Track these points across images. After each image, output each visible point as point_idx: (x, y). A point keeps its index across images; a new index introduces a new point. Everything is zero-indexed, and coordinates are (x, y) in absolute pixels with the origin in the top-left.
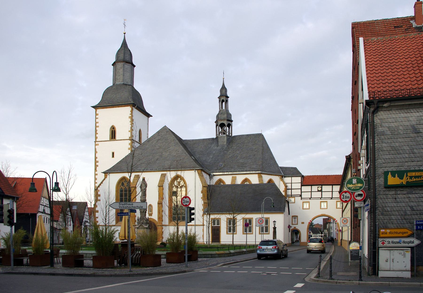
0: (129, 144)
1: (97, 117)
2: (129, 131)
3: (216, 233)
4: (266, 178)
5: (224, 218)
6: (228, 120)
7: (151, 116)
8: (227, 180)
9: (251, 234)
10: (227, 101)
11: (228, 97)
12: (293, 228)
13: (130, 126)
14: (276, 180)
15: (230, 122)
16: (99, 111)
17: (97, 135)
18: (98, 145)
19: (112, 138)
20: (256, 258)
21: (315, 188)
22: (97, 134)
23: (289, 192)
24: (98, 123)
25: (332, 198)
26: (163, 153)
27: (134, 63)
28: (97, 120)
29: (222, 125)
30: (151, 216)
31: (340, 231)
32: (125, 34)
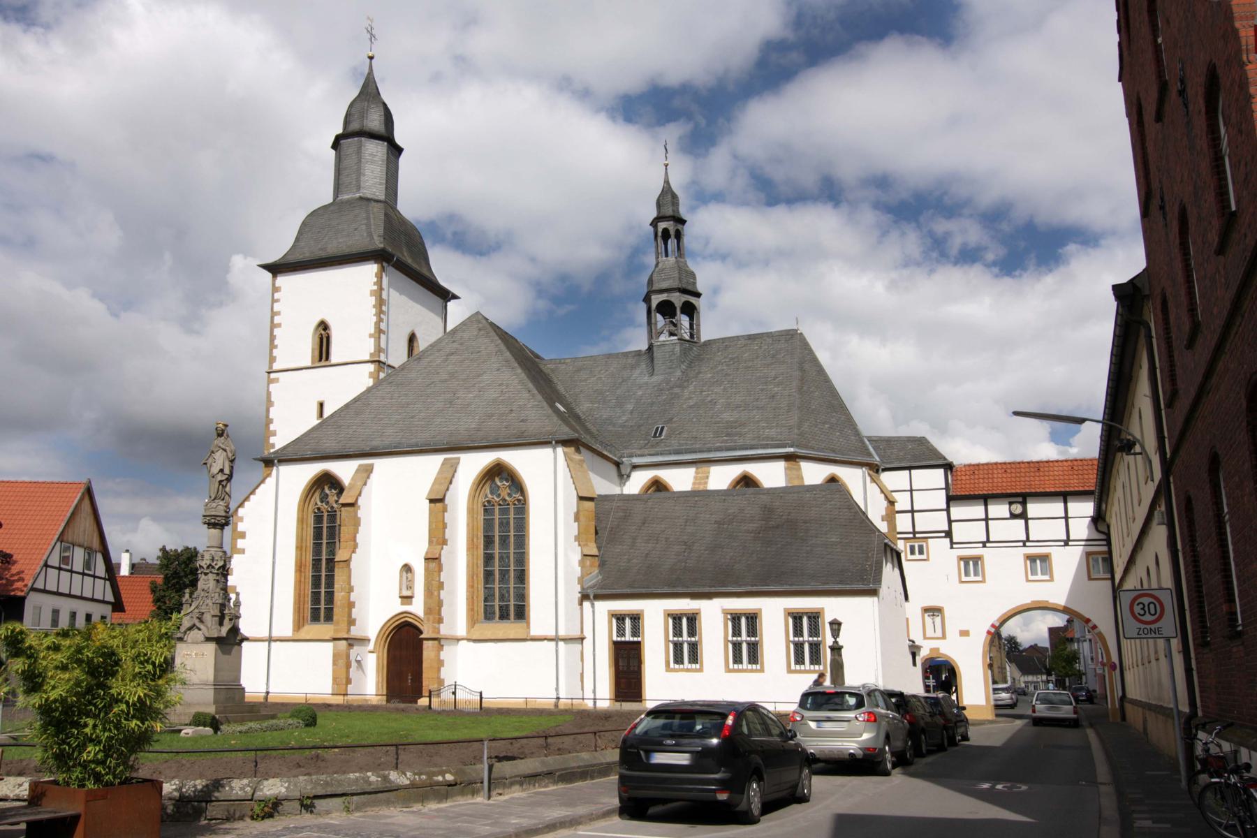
0: (371, 375)
1: (277, 296)
2: (371, 336)
3: (627, 663)
4: (814, 474)
5: (655, 614)
6: (684, 291)
7: (455, 297)
8: (680, 480)
9: (756, 671)
10: (678, 235)
11: (683, 222)
12: (924, 653)
13: (374, 319)
14: (853, 478)
15: (693, 300)
16: (284, 281)
17: (275, 352)
18: (277, 380)
19: (320, 360)
20: (606, 814)
21: (999, 510)
22: (276, 347)
23: (903, 523)
24: (278, 313)
25: (1067, 543)
26: (460, 394)
27: (399, 139)
28: (277, 307)
29: (666, 309)
30: (410, 604)
31: (1113, 667)
32: (371, 58)
